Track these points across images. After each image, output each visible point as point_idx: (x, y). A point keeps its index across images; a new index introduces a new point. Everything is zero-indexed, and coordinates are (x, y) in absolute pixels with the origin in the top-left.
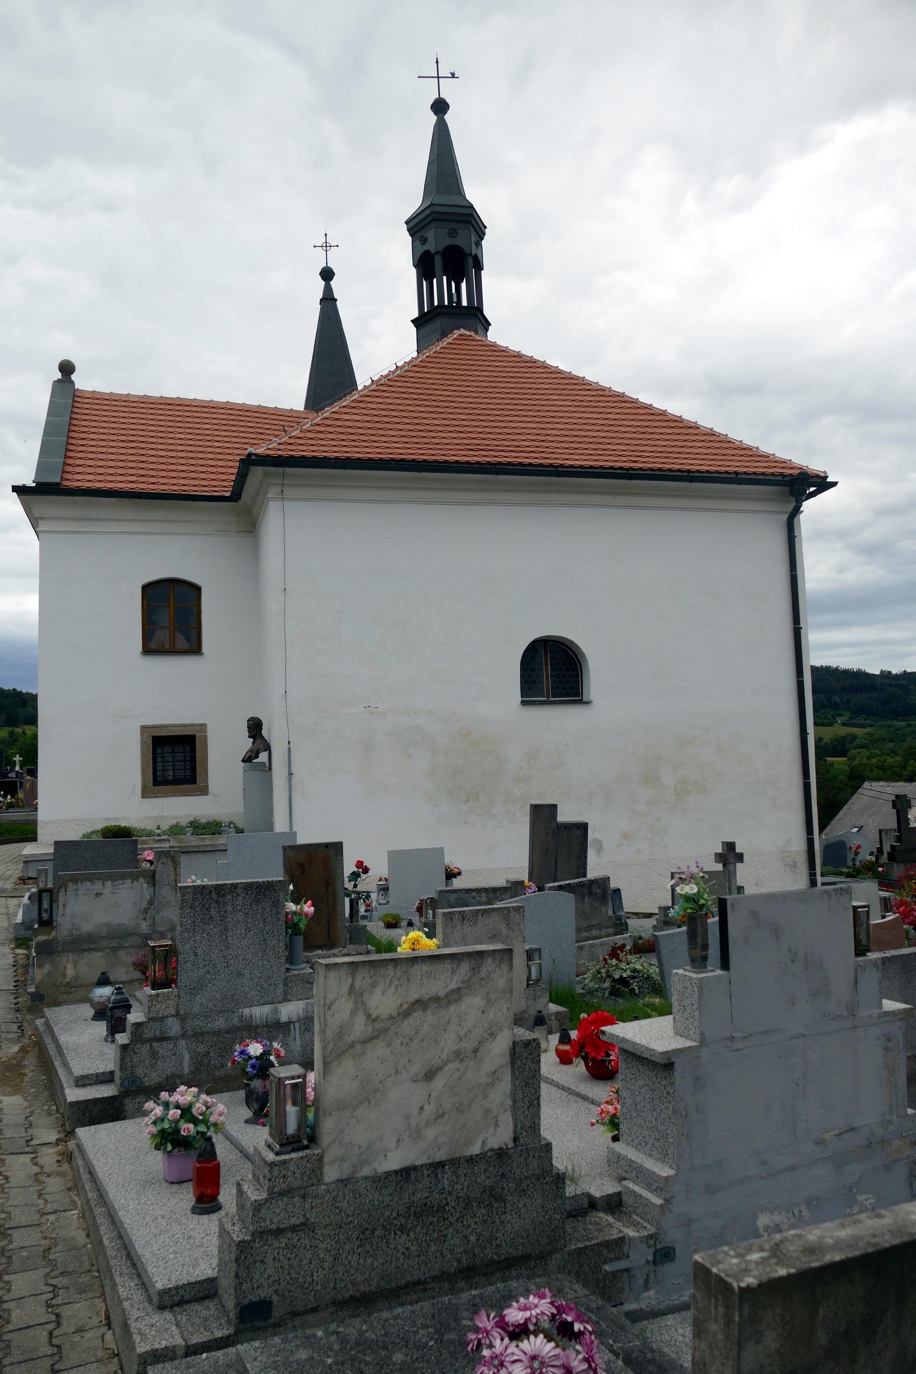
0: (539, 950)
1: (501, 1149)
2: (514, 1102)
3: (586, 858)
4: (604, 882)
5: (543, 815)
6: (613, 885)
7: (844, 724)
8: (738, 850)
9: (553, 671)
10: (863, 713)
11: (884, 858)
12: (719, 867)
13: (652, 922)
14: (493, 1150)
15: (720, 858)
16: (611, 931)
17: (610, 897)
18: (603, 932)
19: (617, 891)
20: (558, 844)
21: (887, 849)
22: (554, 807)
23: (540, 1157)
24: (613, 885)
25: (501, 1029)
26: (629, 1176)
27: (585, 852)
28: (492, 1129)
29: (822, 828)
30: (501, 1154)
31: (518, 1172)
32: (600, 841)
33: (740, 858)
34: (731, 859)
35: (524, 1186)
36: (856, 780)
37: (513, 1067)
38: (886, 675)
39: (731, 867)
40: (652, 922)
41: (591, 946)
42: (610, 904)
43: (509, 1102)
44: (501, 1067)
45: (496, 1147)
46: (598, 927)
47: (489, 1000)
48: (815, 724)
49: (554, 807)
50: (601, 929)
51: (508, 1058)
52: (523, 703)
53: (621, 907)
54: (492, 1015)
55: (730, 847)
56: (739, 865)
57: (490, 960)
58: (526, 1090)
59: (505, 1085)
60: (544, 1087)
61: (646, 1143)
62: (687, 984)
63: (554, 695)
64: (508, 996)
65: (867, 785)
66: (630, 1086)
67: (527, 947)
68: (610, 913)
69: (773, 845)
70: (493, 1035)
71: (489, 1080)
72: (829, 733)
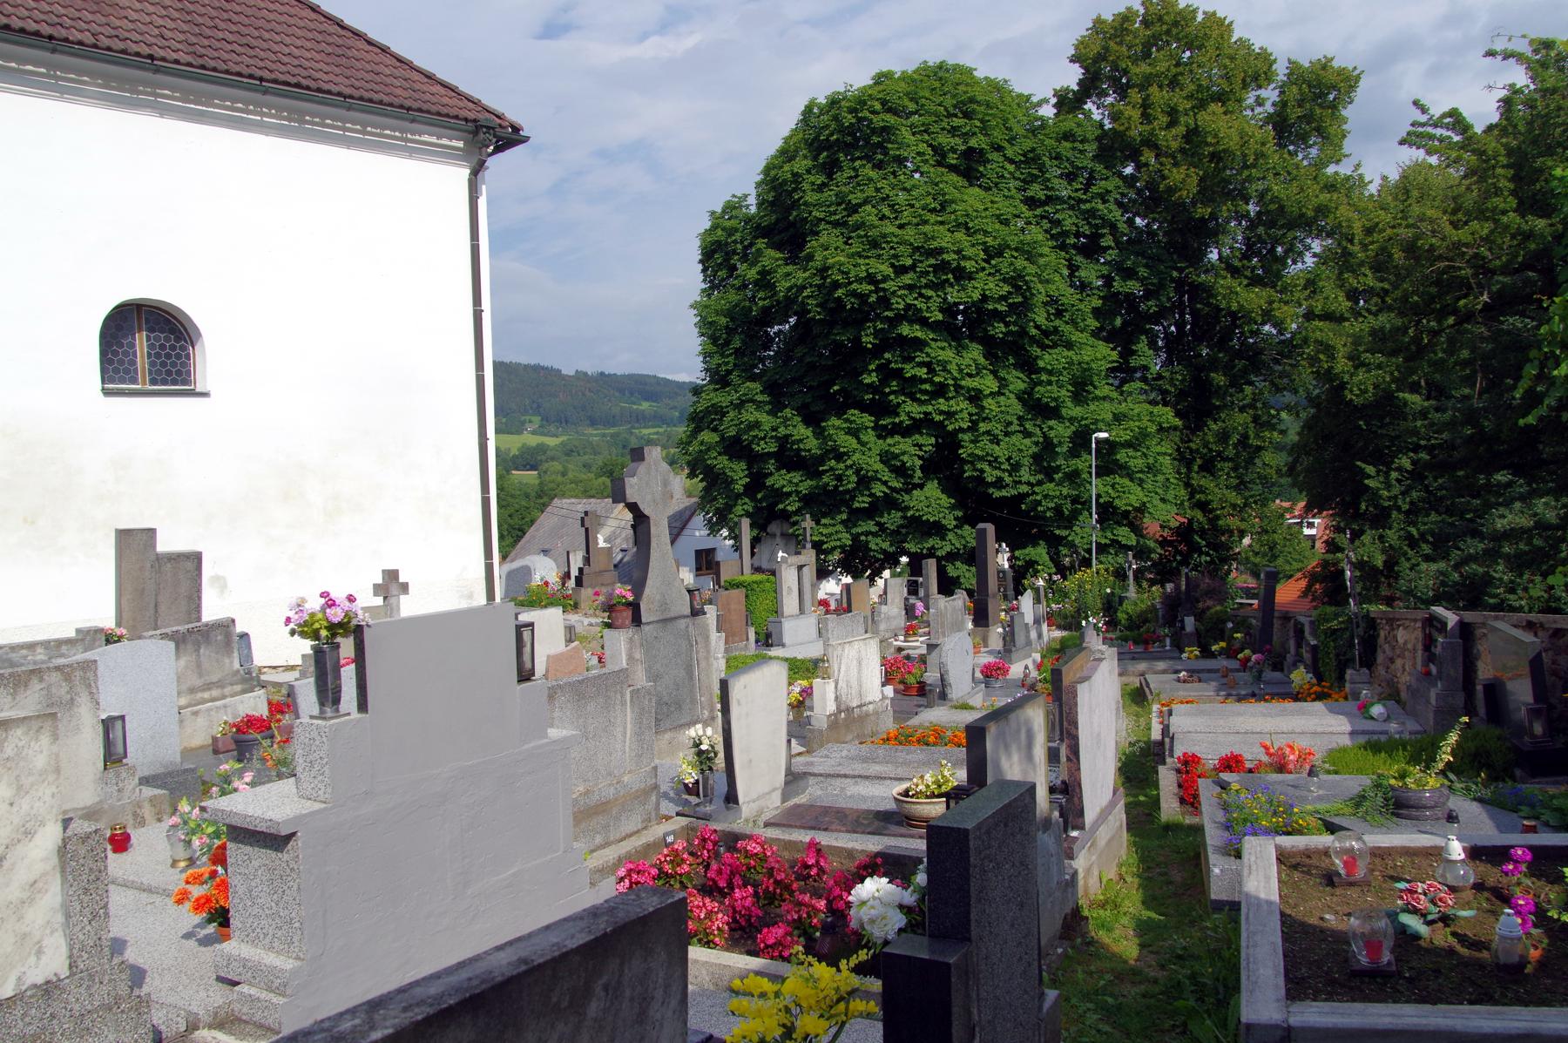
0: (122, 718)
1: (48, 982)
2: (68, 916)
3: (200, 598)
4: (226, 626)
5: (134, 545)
6: (240, 628)
7: (534, 433)
8: (401, 580)
9: (148, 344)
10: (555, 420)
11: (572, 583)
12: (379, 601)
13: (296, 674)
14: (35, 986)
15: (377, 589)
16: (238, 688)
17: (236, 646)
18: (227, 690)
19: (244, 636)
20: (159, 582)
21: (574, 573)
22: (151, 532)
23: (110, 981)
24: (240, 628)
25: (42, 824)
26: (243, 978)
27: (199, 591)
28: (33, 959)
29: (504, 557)
30: (49, 989)
31: (77, 1007)
32: (224, 578)
33: (405, 588)
34: (394, 589)
35: (88, 1022)
36: (543, 497)
37: (63, 871)
38: (581, 376)
39: (393, 600)
40: (296, 674)
41: (209, 710)
42: (236, 654)
43: (60, 918)
44: (44, 874)
45: (40, 980)
46: (220, 684)
47: (20, 788)
48: (497, 431)
49: (151, 532)
50: (223, 687)
51: (55, 860)
52: (107, 393)
53: (249, 657)
54: (25, 807)
55: (391, 575)
56: (402, 597)
57: (19, 732)
58: (86, 899)
59: (53, 895)
60: (111, 887)
61: (265, 935)
62: (315, 734)
63: (154, 382)
64: (51, 778)
65: (556, 502)
66: (242, 870)
67: (104, 717)
68: (237, 665)
69: (443, 559)
70: (29, 834)
71: (25, 895)
72: (515, 443)
